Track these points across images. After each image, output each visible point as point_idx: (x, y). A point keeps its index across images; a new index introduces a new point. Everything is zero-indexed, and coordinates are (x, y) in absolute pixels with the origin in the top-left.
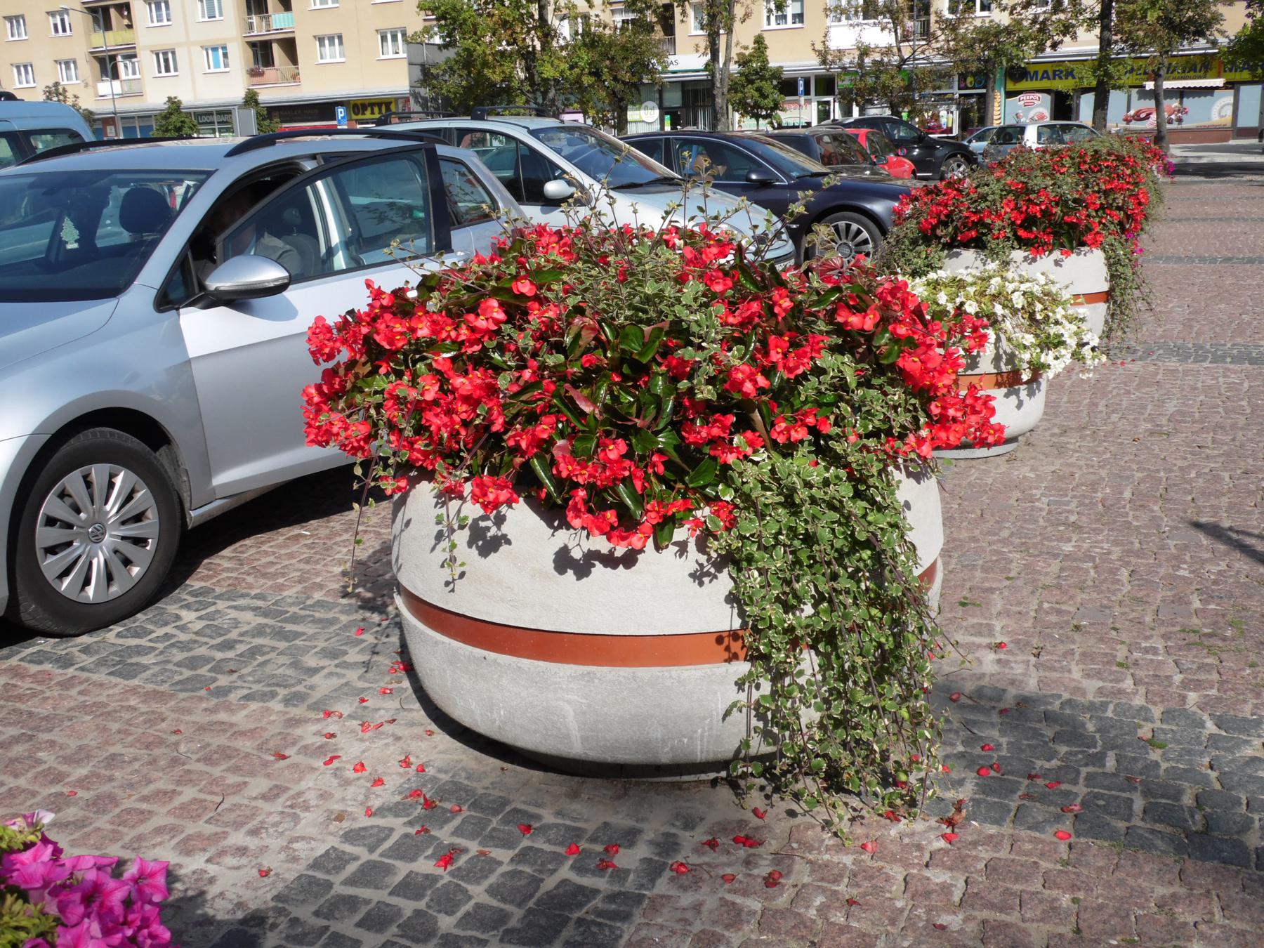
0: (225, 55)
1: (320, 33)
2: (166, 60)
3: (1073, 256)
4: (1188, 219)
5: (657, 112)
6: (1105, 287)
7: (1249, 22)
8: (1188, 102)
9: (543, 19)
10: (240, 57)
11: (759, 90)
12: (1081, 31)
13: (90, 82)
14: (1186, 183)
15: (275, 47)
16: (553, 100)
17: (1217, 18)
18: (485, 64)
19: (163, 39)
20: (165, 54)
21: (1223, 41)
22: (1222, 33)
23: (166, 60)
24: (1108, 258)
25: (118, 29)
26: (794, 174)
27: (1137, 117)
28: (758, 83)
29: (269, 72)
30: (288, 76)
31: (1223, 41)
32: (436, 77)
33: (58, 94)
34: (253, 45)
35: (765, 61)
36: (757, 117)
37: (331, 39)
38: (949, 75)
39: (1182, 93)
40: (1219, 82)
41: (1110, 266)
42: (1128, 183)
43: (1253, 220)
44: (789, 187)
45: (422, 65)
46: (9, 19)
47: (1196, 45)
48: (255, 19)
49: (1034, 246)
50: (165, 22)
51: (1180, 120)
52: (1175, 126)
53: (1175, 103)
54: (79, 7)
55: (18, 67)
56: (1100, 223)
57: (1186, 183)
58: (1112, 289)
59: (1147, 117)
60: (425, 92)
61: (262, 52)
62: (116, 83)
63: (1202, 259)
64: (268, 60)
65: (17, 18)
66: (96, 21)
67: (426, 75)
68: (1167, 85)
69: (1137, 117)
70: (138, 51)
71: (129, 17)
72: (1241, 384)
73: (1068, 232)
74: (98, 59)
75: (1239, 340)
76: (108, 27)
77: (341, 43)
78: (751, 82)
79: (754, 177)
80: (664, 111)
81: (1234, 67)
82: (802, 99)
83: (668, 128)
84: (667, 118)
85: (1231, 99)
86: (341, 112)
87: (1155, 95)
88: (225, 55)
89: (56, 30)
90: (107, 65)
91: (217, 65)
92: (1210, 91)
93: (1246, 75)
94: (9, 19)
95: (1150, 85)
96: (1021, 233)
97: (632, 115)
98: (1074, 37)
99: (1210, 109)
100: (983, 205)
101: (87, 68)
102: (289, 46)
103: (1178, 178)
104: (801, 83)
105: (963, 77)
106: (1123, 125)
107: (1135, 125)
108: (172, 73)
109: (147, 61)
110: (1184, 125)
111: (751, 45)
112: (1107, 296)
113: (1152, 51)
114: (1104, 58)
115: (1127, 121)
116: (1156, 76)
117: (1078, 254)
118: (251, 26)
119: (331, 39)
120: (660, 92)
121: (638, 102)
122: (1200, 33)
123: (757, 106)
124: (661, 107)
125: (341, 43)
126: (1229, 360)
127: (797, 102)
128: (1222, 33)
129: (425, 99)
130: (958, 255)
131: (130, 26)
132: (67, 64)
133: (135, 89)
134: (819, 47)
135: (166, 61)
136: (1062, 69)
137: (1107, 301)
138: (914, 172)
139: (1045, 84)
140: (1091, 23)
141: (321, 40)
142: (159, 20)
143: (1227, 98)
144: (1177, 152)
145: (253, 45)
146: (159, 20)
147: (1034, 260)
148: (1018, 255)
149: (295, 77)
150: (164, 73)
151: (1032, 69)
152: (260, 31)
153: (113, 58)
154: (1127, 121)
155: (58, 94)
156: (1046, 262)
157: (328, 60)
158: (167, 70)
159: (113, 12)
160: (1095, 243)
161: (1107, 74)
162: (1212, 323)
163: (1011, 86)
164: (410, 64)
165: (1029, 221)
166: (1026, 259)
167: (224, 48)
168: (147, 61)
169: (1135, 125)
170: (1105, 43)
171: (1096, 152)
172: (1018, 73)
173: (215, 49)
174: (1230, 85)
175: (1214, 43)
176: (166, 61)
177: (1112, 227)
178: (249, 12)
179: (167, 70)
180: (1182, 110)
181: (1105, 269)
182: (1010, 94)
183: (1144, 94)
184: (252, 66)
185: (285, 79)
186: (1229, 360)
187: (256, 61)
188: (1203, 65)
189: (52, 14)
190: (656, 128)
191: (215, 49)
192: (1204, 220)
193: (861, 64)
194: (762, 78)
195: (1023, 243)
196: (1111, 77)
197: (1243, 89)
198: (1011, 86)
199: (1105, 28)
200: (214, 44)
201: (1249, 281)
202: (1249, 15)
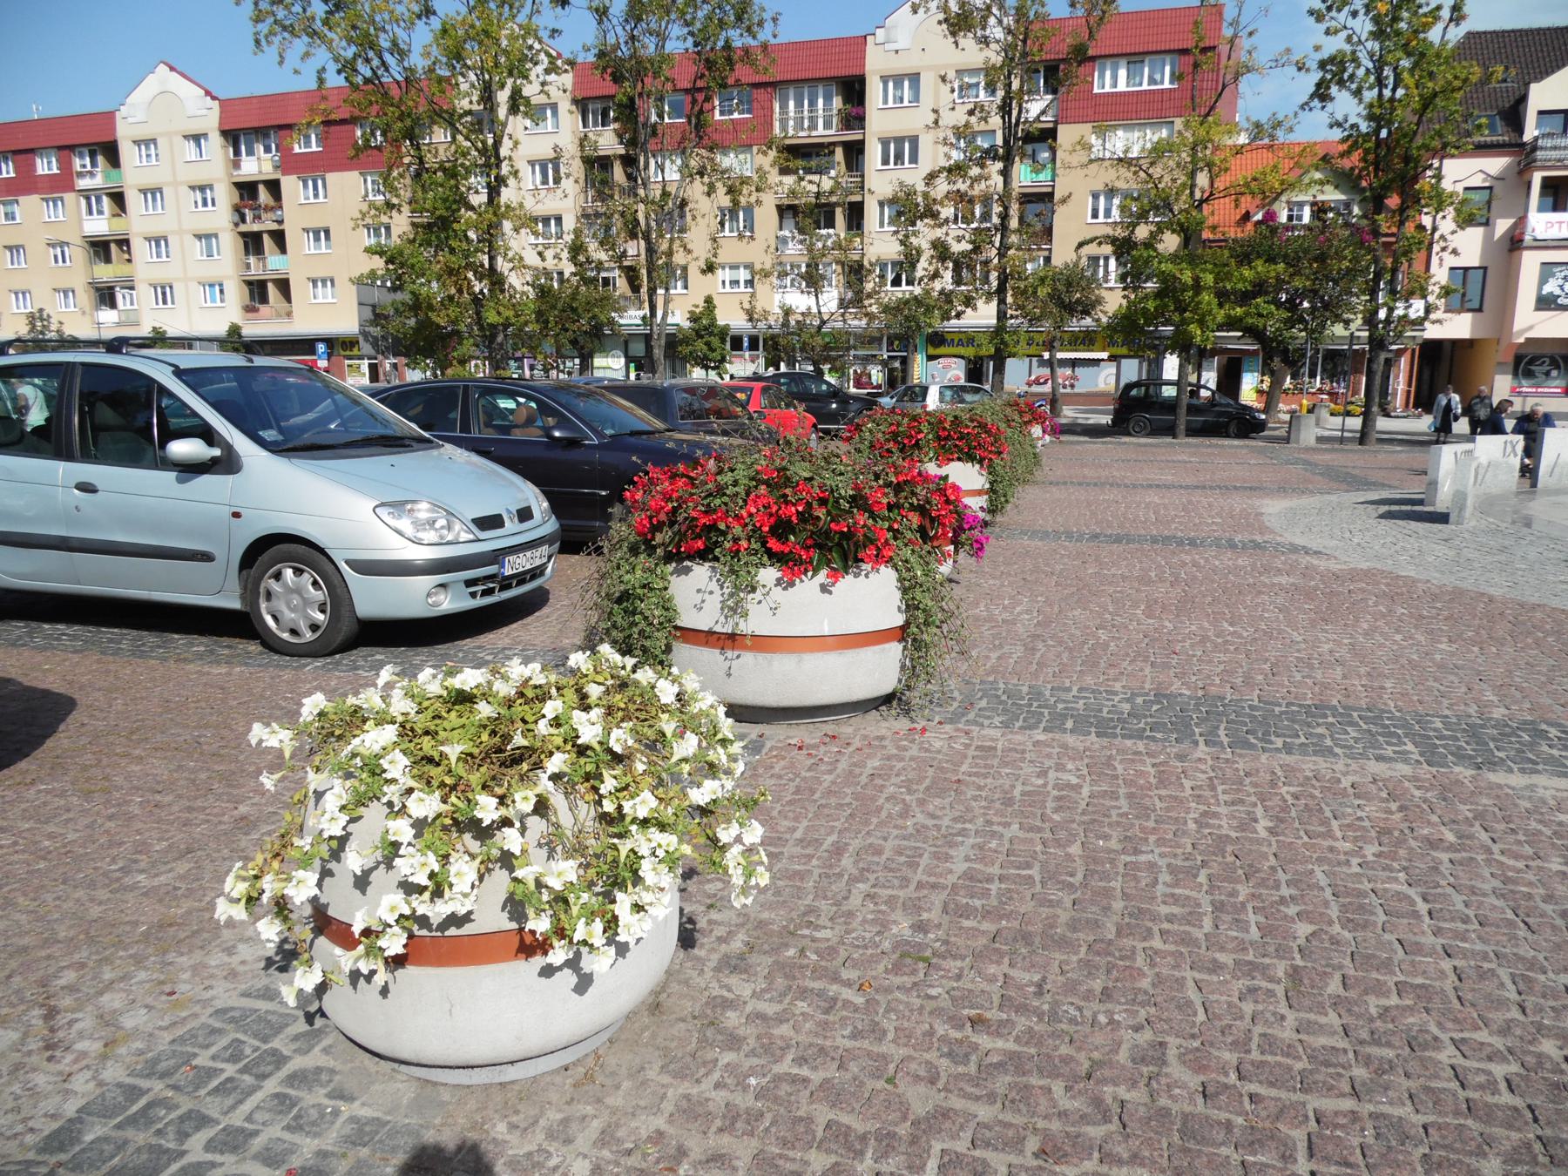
0: (222, 291)
1: (314, 276)
2: (164, 292)
3: (849, 578)
4: (1065, 483)
5: (623, 360)
6: (899, 620)
7: (1124, 302)
8: (1079, 371)
9: (492, 268)
10: (235, 295)
11: (708, 344)
12: (980, 303)
13: (87, 309)
14: (1072, 443)
15: (270, 286)
16: (501, 345)
17: (1099, 301)
18: (431, 307)
19: (161, 275)
20: (163, 288)
21: (1104, 320)
22: (1105, 313)
23: (164, 292)
24: (901, 580)
25: (119, 262)
26: (609, 432)
27: (1037, 382)
28: (707, 338)
29: (263, 309)
30: (283, 313)
31: (1104, 320)
32: (386, 317)
33: (42, 319)
34: (249, 283)
35: (714, 319)
36: (707, 368)
37: (324, 281)
38: (880, 340)
39: (1074, 363)
40: (1105, 355)
41: (905, 591)
42: (286, 699)
43: (1126, 486)
44: (600, 447)
45: (374, 306)
46: (10, 248)
47: (1083, 322)
48: (252, 260)
49: (792, 566)
50: (164, 258)
51: (1072, 386)
52: (1068, 390)
53: (1068, 372)
54: (79, 242)
55: (16, 294)
56: (890, 529)
57: (1072, 443)
58: (907, 624)
59: (1045, 382)
60: (376, 331)
61: (257, 291)
62: (114, 312)
63: (1070, 536)
64: (264, 299)
65: (17, 248)
66: (97, 254)
67: (378, 317)
68: (1060, 355)
69: (1037, 382)
70: (136, 284)
71: (129, 252)
72: (1079, 786)
73: (839, 545)
74: (97, 289)
75: (1089, 680)
76: (108, 260)
77: (333, 284)
78: (702, 337)
79: (557, 434)
80: (629, 359)
81: (1113, 343)
82: (747, 354)
83: (632, 376)
84: (632, 365)
85: (1114, 370)
86: (321, 348)
87: (1050, 363)
88: (222, 291)
89: (56, 261)
90: (106, 296)
91: (213, 301)
92: (1096, 362)
93: (1124, 351)
94: (10, 248)
95: (1046, 355)
96: (773, 544)
97: (598, 361)
98: (975, 308)
99: (1097, 376)
100: (718, 502)
101: (85, 297)
102: (284, 286)
103: (1064, 438)
104: (1399, 401)
105: (890, 343)
106: (1026, 388)
107: (1036, 389)
108: (170, 305)
109: (145, 294)
110: (1076, 390)
111: (702, 304)
112: (901, 633)
113: (1046, 326)
114: (1000, 330)
115: (1029, 385)
116: (1050, 346)
117: (856, 575)
118: (248, 266)
119: (324, 281)
120: (626, 343)
121: (604, 351)
122: (1087, 313)
123: (706, 358)
124: (626, 356)
125: (333, 284)
126: (1069, 724)
127: (742, 357)
128: (1105, 313)
129: (375, 338)
130: (688, 570)
131: (129, 261)
132: (65, 293)
133: (132, 317)
134: (747, 306)
135: (164, 294)
136: (968, 338)
137: (902, 639)
138: (815, 426)
139: (962, 351)
140: (989, 296)
141: (314, 282)
142: (159, 255)
143: (1109, 370)
144: (1069, 413)
145: (249, 283)
146: (159, 255)
147: (791, 584)
148: (768, 575)
149: (289, 314)
150: (161, 305)
151: (949, 337)
152: (256, 271)
153: (112, 288)
154: (1029, 385)
155: (42, 319)
156: (808, 586)
157: (320, 300)
158: (165, 302)
159: (113, 247)
160: (880, 559)
161: (1003, 342)
162: (1060, 643)
163: (932, 351)
164: (360, 304)
165: (782, 528)
166: (779, 582)
167: (221, 285)
168: (145, 294)
169: (1036, 389)
170: (1001, 316)
171: (956, 417)
172: (937, 339)
173: (212, 285)
174: (1112, 358)
175: (1098, 320)
176: (164, 294)
177: (909, 535)
178: (247, 252)
179: (165, 302)
180: (1074, 378)
181: (898, 594)
182: (931, 358)
183: (1042, 363)
184: (248, 302)
185: (279, 316)
186: (1069, 724)
187: (252, 297)
188: (1086, 339)
189: (53, 246)
190: (620, 375)
191: (212, 285)
192: (1080, 484)
193: (786, 324)
194: (711, 334)
195: (776, 558)
196: (1006, 345)
197: (1124, 361)
198: (932, 351)
199: (1002, 301)
200: (212, 281)
201: (1113, 571)
202: (1124, 297)
